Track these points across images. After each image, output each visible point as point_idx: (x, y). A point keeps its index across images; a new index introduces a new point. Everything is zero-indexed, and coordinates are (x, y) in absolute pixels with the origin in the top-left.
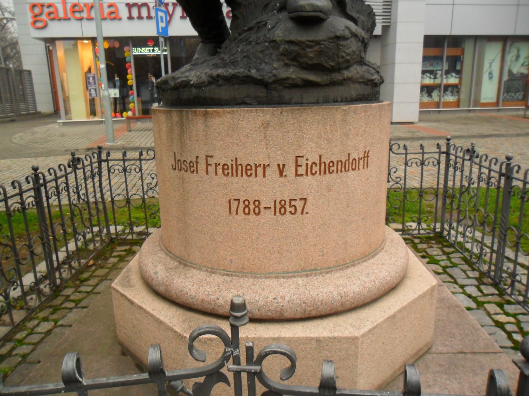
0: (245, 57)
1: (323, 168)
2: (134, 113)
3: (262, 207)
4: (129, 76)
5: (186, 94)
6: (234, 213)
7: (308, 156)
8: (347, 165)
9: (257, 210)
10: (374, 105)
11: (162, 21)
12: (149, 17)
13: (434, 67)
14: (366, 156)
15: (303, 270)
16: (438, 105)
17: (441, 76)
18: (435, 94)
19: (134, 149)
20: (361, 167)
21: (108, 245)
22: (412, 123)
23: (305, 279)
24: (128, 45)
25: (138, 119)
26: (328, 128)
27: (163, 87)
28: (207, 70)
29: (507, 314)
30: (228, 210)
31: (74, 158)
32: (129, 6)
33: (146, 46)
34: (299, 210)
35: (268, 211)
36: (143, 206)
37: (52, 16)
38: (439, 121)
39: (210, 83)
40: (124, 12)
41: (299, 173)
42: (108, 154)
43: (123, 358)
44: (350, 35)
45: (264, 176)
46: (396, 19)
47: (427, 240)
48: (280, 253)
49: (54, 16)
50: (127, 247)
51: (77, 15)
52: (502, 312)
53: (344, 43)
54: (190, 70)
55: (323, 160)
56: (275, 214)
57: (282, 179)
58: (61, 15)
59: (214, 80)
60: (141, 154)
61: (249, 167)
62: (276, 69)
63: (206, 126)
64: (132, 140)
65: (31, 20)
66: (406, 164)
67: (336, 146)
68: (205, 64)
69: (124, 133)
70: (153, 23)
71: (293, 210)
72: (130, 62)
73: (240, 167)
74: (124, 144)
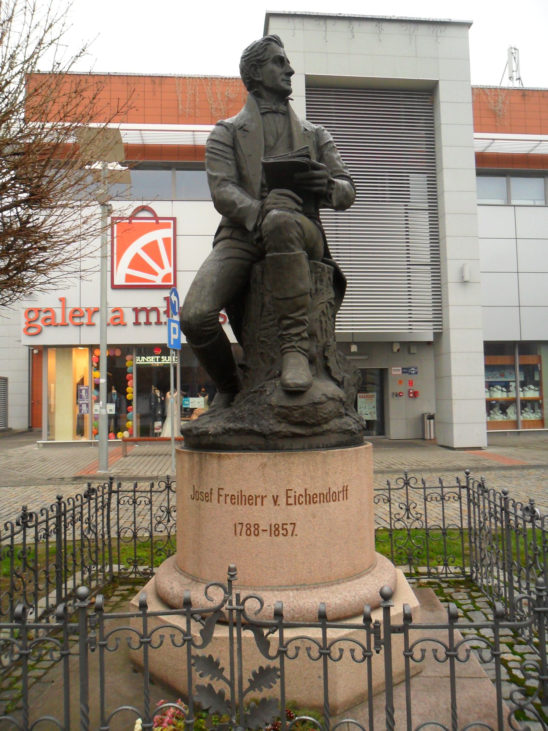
0: (250, 414)
1: (308, 499)
2: (131, 435)
3: (260, 529)
4: (129, 389)
5: (205, 441)
6: (238, 534)
7: (296, 490)
8: (328, 497)
9: (256, 532)
10: (349, 449)
11: (175, 333)
12: (158, 323)
13: (506, 378)
14: (345, 490)
15: (294, 585)
16: (515, 424)
17: (516, 388)
18: (511, 411)
19: (130, 479)
20: (341, 499)
21: (109, 584)
22: (480, 448)
23: (295, 592)
24: (132, 354)
25: (135, 441)
26: (311, 468)
27: (188, 433)
28: (222, 424)
29: (514, 653)
30: (234, 531)
31: (89, 489)
32: (137, 311)
33: (151, 355)
34: (290, 532)
35: (265, 533)
36: (149, 542)
37: (49, 322)
38: (515, 446)
39: (223, 433)
40: (130, 317)
41: (289, 503)
42: (119, 485)
43: (135, 675)
44: (326, 400)
45: (262, 504)
46: (448, 325)
47: (455, 584)
48: (275, 569)
49: (50, 322)
50: (130, 587)
51: (77, 321)
52: (510, 651)
53: (321, 406)
54: (210, 422)
55: (308, 493)
56: (271, 536)
57: (276, 507)
58: (59, 320)
59: (227, 432)
60: (152, 485)
61: (251, 498)
62: (271, 424)
63: (220, 466)
64: (129, 468)
65: (24, 326)
66: (426, 499)
67: (318, 482)
68: (220, 417)
69: (118, 458)
70: (163, 330)
71: (284, 532)
72: (132, 373)
73: (244, 497)
74: (119, 473)
